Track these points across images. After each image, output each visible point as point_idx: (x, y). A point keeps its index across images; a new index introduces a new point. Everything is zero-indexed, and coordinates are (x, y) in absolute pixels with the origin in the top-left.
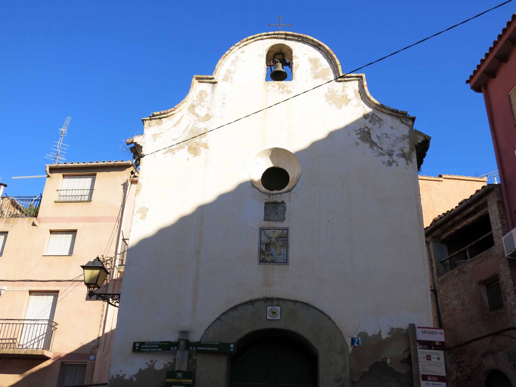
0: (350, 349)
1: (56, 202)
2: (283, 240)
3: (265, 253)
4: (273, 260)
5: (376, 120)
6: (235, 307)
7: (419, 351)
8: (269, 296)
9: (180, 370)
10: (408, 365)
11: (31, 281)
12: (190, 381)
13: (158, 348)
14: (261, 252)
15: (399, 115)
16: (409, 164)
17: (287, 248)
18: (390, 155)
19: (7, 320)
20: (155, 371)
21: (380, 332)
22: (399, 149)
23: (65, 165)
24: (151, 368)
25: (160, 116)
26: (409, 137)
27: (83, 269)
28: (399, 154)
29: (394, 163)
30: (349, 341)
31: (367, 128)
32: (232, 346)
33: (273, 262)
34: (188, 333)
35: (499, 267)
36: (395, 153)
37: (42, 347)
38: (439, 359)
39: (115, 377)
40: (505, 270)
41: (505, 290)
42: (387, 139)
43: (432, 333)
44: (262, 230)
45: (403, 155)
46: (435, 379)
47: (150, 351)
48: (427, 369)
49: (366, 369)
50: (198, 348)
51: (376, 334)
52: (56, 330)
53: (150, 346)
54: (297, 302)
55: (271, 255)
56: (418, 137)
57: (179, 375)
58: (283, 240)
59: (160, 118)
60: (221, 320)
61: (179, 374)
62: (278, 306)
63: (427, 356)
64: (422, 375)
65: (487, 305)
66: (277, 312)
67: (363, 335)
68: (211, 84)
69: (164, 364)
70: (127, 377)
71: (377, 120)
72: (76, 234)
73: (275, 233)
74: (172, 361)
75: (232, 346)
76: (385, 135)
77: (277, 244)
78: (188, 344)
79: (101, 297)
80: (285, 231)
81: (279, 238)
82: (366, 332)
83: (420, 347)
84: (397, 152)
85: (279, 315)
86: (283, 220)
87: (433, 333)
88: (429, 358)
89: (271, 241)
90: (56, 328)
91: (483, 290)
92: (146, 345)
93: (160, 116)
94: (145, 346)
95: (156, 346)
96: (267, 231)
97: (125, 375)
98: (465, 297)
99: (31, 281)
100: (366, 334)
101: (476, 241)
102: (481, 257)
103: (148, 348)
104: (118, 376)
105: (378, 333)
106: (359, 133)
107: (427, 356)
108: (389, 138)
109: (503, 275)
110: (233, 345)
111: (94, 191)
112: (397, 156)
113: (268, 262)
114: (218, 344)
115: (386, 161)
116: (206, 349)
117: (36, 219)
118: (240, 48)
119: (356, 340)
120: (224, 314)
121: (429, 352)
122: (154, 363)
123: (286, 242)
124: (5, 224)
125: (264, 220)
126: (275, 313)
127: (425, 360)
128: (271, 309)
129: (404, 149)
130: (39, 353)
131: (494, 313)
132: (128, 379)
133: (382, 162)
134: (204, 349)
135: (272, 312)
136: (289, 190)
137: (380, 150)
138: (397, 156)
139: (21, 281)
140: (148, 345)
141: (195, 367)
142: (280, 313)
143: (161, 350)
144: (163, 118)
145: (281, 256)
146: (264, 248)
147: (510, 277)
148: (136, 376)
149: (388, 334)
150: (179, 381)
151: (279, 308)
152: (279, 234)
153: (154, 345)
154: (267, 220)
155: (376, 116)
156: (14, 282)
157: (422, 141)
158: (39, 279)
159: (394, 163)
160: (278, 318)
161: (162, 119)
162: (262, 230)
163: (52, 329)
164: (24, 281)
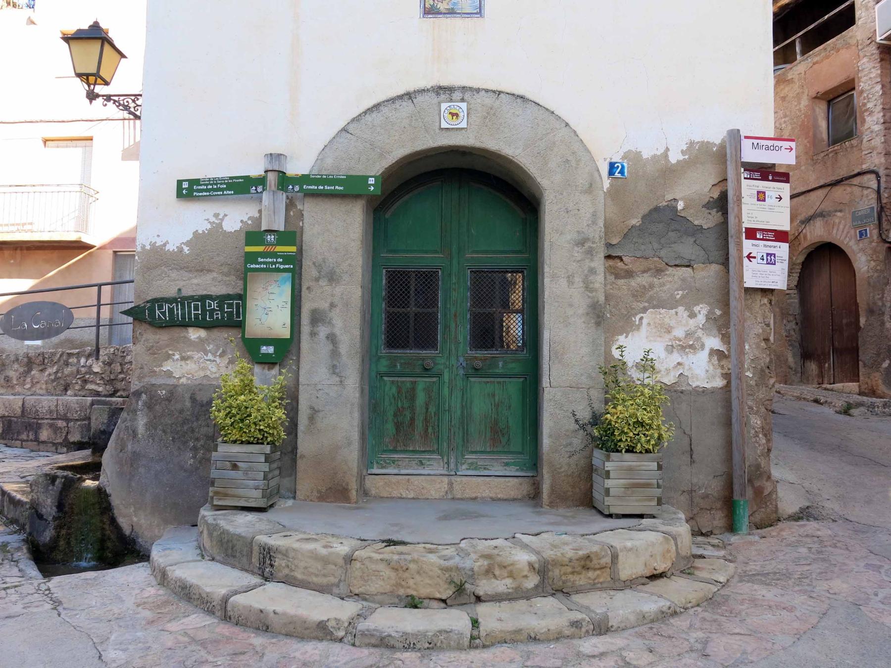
0: (607, 183)
4: (453, 9)
6: (377, 107)
7: (744, 183)
9: (270, 229)
10: (717, 212)
12: (293, 249)
13: (226, 189)
20: (225, 233)
21: (667, 149)
27: (66, 45)
30: (604, 169)
32: (371, 181)
34: (282, 156)
35: (859, 65)
38: (781, 198)
39: (148, 247)
40: (870, 69)
41: (864, 105)
43: (772, 148)
46: (771, 236)
47: (210, 195)
48: (756, 217)
49: (635, 221)
50: (304, 186)
51: (659, 153)
53: (210, 187)
54: (500, 92)
57: (270, 238)
60: (348, 132)
61: (269, 237)
62: (463, 100)
63: (758, 192)
64: (746, 228)
65: (825, 136)
66: (461, 115)
67: (634, 157)
69: (242, 221)
70: (171, 247)
74: (257, 215)
75: (371, 181)
78: (284, 181)
79: (112, 101)
82: (638, 150)
83: (746, 176)
87: (774, 148)
88: (761, 197)
91: (821, 109)
92: (201, 185)
94: (199, 187)
95: (222, 186)
97: (167, 243)
98: (783, 125)
100: (638, 154)
101: (816, 23)
102: (825, 49)
103: (207, 190)
104: (153, 245)
105: (662, 151)
107: (758, 192)
109: (863, 79)
110: (373, 179)
113: (441, 13)
114: (343, 177)
119: (618, 167)
120: (356, 119)
121: (762, 185)
122: (222, 220)
126: (457, 115)
128: (449, 108)
131: (836, 148)
132: (174, 250)
134: (316, 188)
135: (450, 113)
140: (207, 185)
141: (301, 224)
142: (468, 114)
143: (232, 192)
147: (879, 80)
148: (188, 243)
149: (683, 152)
150: (270, 249)
151: (464, 105)
153: (216, 184)
160: (464, 125)
163: (90, 201)
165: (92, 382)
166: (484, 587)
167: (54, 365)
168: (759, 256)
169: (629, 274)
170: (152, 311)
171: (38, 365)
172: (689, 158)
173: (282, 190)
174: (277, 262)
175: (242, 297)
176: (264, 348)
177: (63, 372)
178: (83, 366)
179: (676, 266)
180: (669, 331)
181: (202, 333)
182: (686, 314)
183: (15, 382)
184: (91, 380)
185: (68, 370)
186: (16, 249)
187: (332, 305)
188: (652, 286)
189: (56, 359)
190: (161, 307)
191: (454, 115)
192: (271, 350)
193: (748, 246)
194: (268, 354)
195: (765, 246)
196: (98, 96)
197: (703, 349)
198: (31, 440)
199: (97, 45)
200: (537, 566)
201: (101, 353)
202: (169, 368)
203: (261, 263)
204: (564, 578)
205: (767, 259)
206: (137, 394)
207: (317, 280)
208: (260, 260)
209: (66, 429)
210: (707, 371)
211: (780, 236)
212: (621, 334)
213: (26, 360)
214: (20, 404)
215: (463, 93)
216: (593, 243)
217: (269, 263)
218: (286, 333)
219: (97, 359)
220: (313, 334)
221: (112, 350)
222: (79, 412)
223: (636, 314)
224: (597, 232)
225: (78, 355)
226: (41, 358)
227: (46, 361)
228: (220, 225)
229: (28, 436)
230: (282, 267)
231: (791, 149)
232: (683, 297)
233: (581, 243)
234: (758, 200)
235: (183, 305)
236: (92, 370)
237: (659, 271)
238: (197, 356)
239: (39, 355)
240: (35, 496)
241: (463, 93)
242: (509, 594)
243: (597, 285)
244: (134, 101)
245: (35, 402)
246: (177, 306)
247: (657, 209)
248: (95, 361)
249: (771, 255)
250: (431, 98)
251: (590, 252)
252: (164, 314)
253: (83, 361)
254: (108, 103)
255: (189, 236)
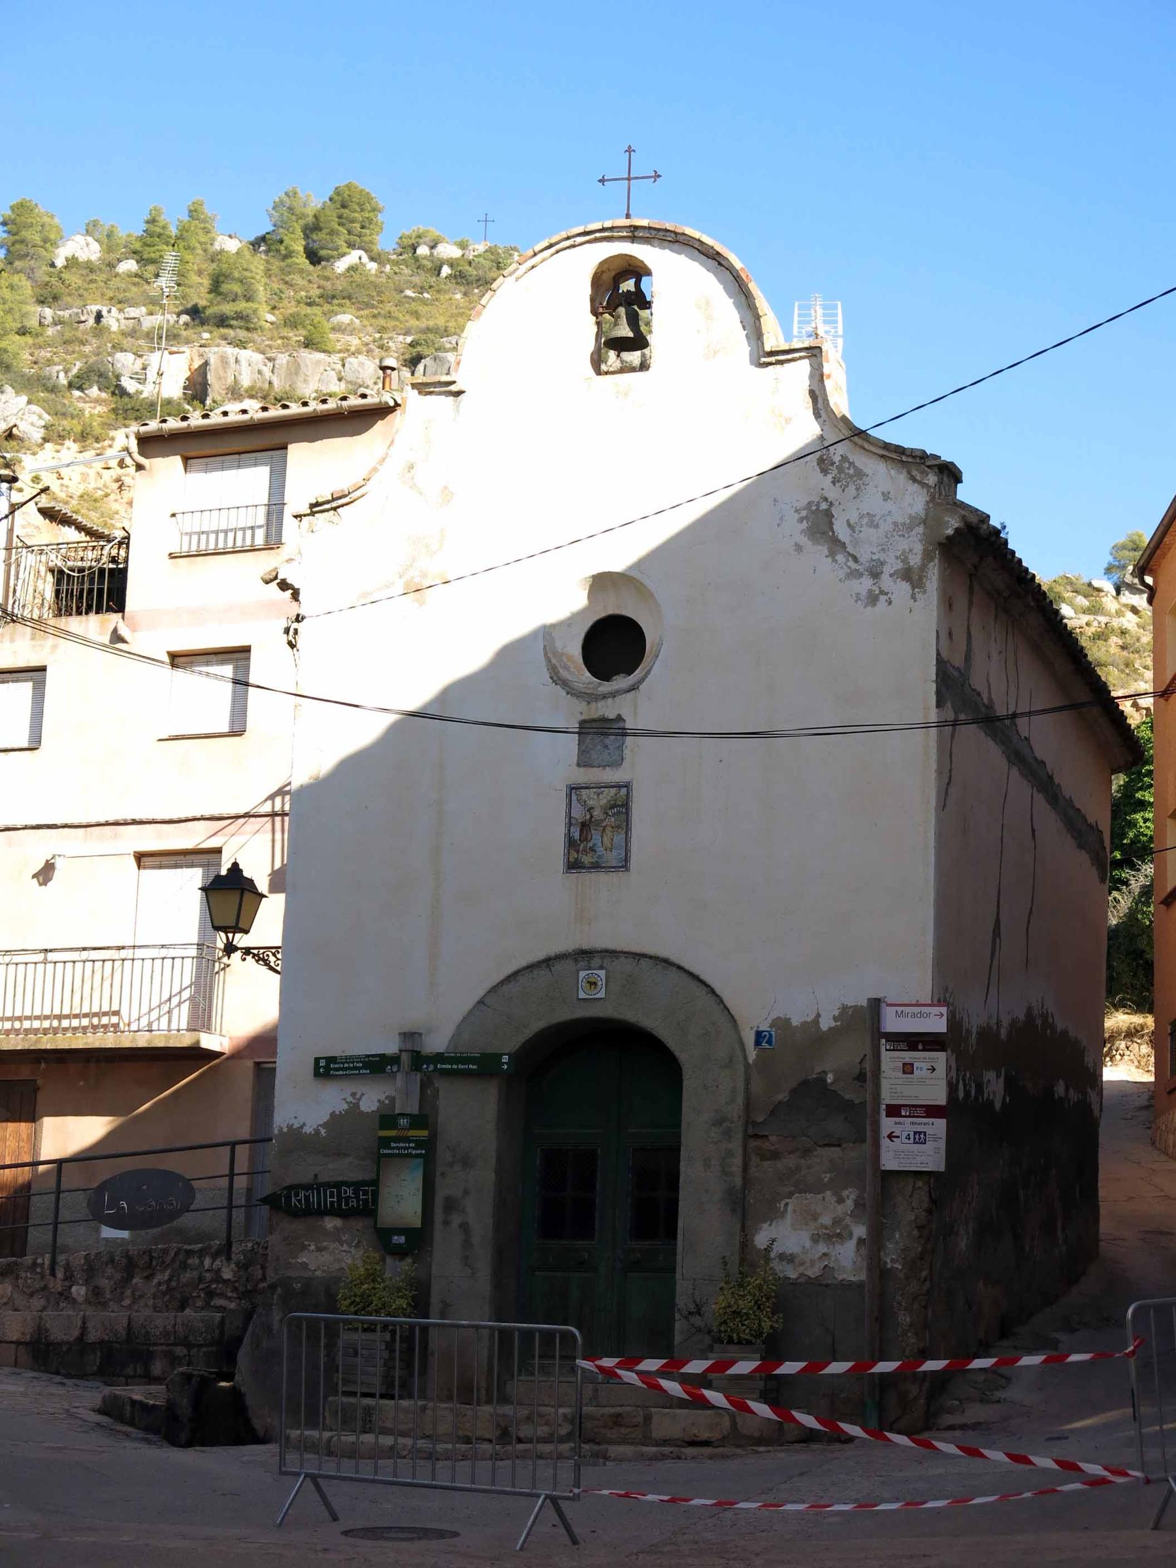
0: (752, 1054)
1: (172, 556)
2: (619, 813)
3: (579, 845)
5: (848, 474)
8: (585, 946)
11: (134, 822)
12: (425, 1133)
14: (571, 843)
15: (904, 459)
16: (918, 596)
17: (626, 833)
18: (875, 575)
19: (84, 949)
21: (818, 1015)
22: (897, 558)
23: (185, 424)
24: (354, 1107)
25: (334, 504)
26: (924, 522)
28: (896, 572)
29: (883, 598)
30: (749, 1038)
31: (826, 499)
32: (505, 1059)
33: (596, 866)
36: (887, 570)
37: (184, 1025)
38: (934, 1069)
39: (285, 1130)
42: (872, 530)
44: (573, 789)
45: (907, 574)
49: (782, 1096)
52: (227, 969)
53: (346, 1065)
54: (644, 956)
55: (592, 849)
56: (946, 519)
57: (403, 1122)
58: (619, 813)
59: (335, 509)
62: (601, 968)
63: (904, 1064)
64: (887, 1105)
66: (600, 983)
67: (782, 1024)
68: (451, 398)
70: (308, 1130)
71: (851, 477)
72: (248, 659)
73: (601, 796)
75: (505, 1059)
76: (866, 520)
77: (604, 824)
78: (418, 1060)
80: (624, 791)
81: (611, 808)
84: (893, 565)
85: (604, 989)
86: (618, 763)
89: (592, 817)
90: (228, 966)
93: (334, 504)
96: (584, 792)
97: (304, 1124)
99: (134, 822)
100: (788, 1021)
103: (346, 1069)
104: (290, 1127)
106: (806, 517)
107: (904, 1064)
108: (877, 526)
111: (286, 507)
112: (891, 575)
113: (584, 868)
115: (864, 593)
116: (455, 1067)
117: (123, 618)
118: (517, 279)
120: (493, 990)
121: (908, 1056)
122: (359, 1099)
123: (624, 816)
124: (33, 642)
125: (578, 765)
126: (595, 984)
127: (900, 1074)
129: (910, 557)
130: (186, 1040)
133: (854, 595)
136: (633, 685)
137: (851, 563)
138: (891, 575)
139: (107, 824)
144: (342, 506)
145: (615, 853)
146: (577, 836)
148: (325, 1125)
149: (835, 1019)
151: (602, 973)
152: (609, 798)
153: (353, 1063)
154: (585, 766)
155: (852, 464)
156: (88, 829)
157: (957, 530)
158: (159, 817)
159: (883, 598)
160: (602, 995)
161: (339, 510)
162: (574, 791)
163: (216, 969)
164: (116, 824)
165: (222, 1295)
166: (526, 1431)
167: (165, 1269)
168: (905, 1135)
169: (775, 1156)
170: (288, 1198)
171: (143, 1269)
172: (842, 1024)
173: (416, 1070)
174: (409, 1148)
175: (375, 1183)
176: (396, 1237)
177: (178, 1280)
178: (208, 1271)
179: (826, 1145)
180: (815, 1218)
181: (338, 1222)
182: (834, 1199)
183: (108, 1296)
184: (218, 1291)
185: (187, 1276)
186: (88, 1061)
187: (466, 1192)
188: (798, 1168)
189: (168, 1259)
190: (297, 1195)
191: (593, 984)
192: (401, 1239)
193: (887, 1124)
194: (399, 1244)
195: (913, 1123)
196: (236, 949)
197: (851, 1239)
198: (140, 1376)
199: (234, 897)
200: (569, 1417)
201: (234, 1249)
202: (304, 1260)
203: (394, 1148)
204: (596, 1430)
205: (915, 1139)
206: (273, 1287)
207: (451, 1165)
208: (393, 1145)
209: (187, 1358)
210: (855, 1262)
211: (932, 1111)
212: (765, 1222)
213: (124, 1261)
214: (125, 1322)
215: (602, 958)
216: (732, 1122)
217: (402, 1148)
218: (417, 1223)
219: (229, 1259)
220: (446, 1223)
221: (250, 1245)
222: (204, 1335)
223: (781, 1200)
224: (736, 1110)
225: (201, 1253)
226: (146, 1258)
227: (154, 1263)
228: (357, 1106)
229: (135, 1370)
230: (414, 1152)
231: (942, 1015)
232: (831, 1179)
233: (719, 1122)
234: (904, 1072)
235: (319, 1193)
236: (221, 1277)
237: (807, 1152)
238: (333, 1246)
239: (144, 1253)
240: (171, 1396)
241: (602, 958)
242: (544, 1438)
243: (734, 1169)
244: (274, 955)
245: (146, 1321)
246: (313, 1193)
247: (805, 1083)
248: (224, 1262)
249: (920, 1133)
250: (569, 965)
251: (728, 1134)
252: (300, 1201)
253: (207, 1262)
254: (247, 957)
255: (326, 1118)
